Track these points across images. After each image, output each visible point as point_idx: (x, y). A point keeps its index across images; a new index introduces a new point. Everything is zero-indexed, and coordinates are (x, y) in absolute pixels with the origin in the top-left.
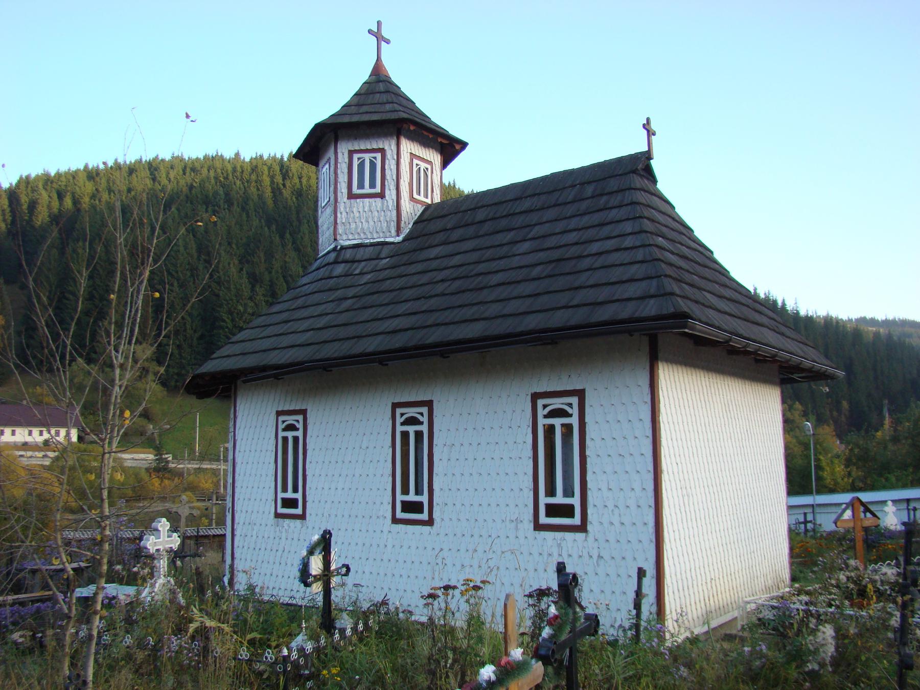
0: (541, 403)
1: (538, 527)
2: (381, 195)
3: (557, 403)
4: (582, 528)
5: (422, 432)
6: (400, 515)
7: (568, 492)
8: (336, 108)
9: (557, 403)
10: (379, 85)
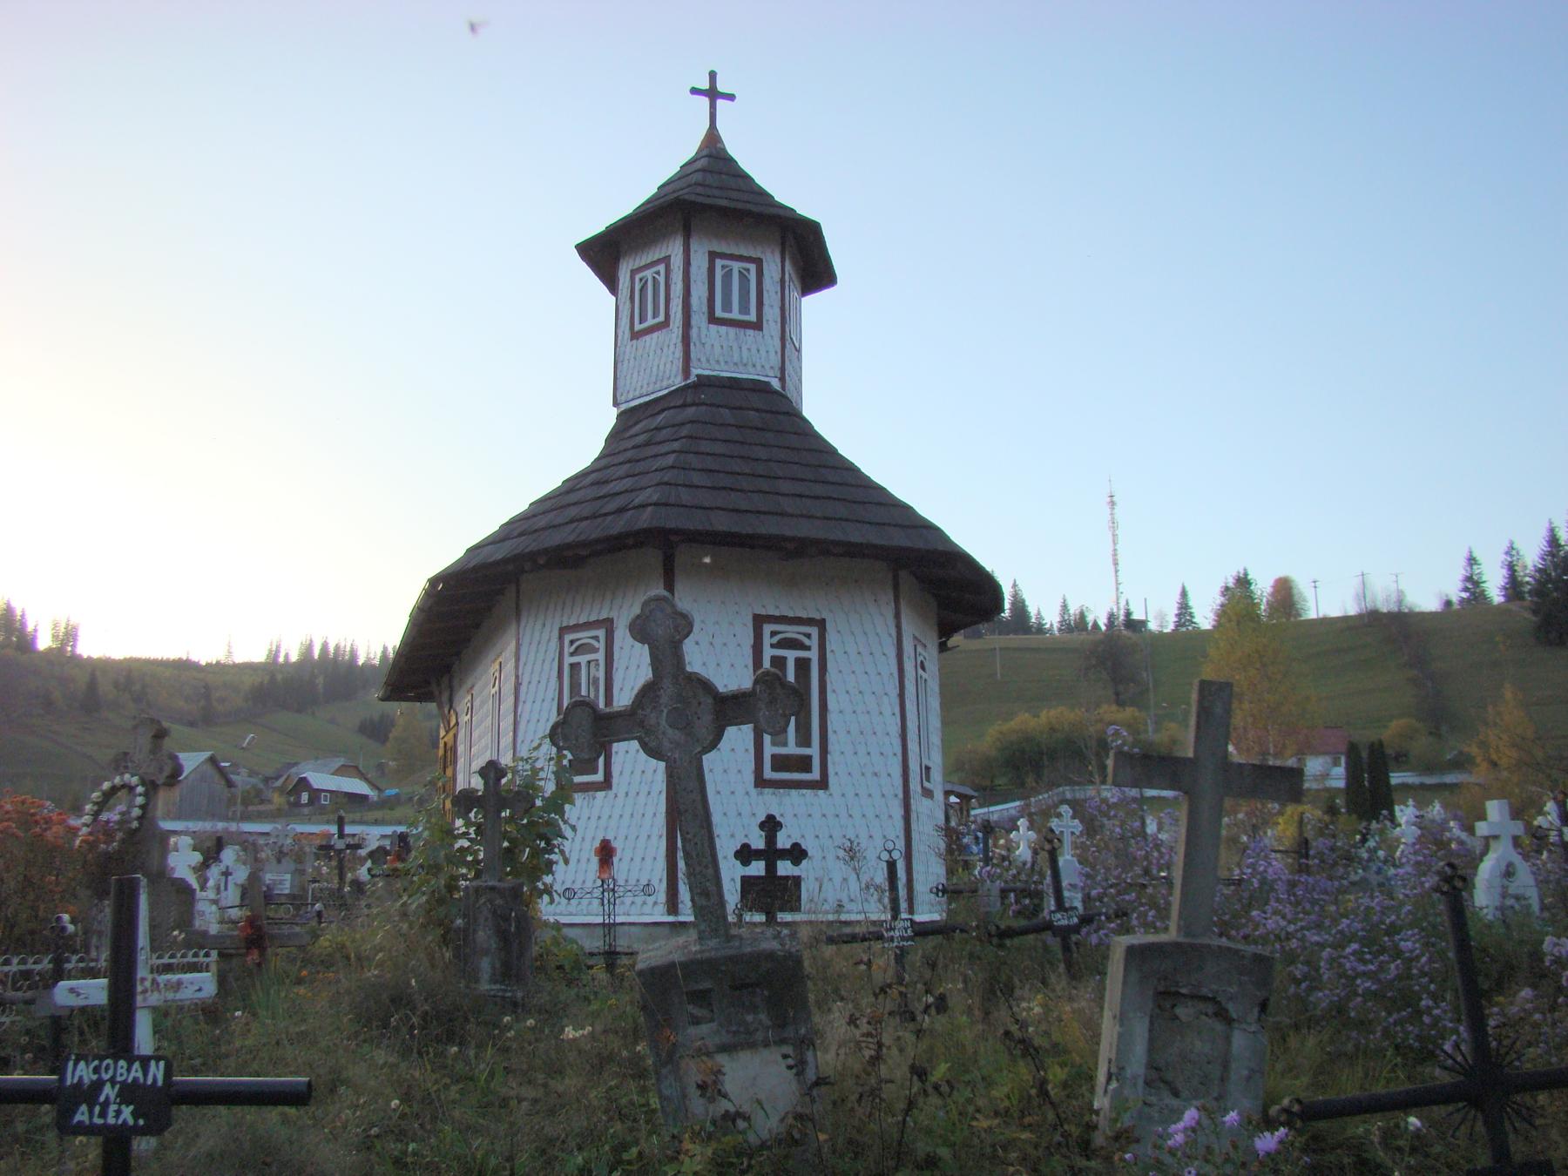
2: (758, 326)
3: (791, 631)
4: (822, 784)
5: (808, 660)
8: (651, 190)
9: (791, 631)
10: (714, 159)
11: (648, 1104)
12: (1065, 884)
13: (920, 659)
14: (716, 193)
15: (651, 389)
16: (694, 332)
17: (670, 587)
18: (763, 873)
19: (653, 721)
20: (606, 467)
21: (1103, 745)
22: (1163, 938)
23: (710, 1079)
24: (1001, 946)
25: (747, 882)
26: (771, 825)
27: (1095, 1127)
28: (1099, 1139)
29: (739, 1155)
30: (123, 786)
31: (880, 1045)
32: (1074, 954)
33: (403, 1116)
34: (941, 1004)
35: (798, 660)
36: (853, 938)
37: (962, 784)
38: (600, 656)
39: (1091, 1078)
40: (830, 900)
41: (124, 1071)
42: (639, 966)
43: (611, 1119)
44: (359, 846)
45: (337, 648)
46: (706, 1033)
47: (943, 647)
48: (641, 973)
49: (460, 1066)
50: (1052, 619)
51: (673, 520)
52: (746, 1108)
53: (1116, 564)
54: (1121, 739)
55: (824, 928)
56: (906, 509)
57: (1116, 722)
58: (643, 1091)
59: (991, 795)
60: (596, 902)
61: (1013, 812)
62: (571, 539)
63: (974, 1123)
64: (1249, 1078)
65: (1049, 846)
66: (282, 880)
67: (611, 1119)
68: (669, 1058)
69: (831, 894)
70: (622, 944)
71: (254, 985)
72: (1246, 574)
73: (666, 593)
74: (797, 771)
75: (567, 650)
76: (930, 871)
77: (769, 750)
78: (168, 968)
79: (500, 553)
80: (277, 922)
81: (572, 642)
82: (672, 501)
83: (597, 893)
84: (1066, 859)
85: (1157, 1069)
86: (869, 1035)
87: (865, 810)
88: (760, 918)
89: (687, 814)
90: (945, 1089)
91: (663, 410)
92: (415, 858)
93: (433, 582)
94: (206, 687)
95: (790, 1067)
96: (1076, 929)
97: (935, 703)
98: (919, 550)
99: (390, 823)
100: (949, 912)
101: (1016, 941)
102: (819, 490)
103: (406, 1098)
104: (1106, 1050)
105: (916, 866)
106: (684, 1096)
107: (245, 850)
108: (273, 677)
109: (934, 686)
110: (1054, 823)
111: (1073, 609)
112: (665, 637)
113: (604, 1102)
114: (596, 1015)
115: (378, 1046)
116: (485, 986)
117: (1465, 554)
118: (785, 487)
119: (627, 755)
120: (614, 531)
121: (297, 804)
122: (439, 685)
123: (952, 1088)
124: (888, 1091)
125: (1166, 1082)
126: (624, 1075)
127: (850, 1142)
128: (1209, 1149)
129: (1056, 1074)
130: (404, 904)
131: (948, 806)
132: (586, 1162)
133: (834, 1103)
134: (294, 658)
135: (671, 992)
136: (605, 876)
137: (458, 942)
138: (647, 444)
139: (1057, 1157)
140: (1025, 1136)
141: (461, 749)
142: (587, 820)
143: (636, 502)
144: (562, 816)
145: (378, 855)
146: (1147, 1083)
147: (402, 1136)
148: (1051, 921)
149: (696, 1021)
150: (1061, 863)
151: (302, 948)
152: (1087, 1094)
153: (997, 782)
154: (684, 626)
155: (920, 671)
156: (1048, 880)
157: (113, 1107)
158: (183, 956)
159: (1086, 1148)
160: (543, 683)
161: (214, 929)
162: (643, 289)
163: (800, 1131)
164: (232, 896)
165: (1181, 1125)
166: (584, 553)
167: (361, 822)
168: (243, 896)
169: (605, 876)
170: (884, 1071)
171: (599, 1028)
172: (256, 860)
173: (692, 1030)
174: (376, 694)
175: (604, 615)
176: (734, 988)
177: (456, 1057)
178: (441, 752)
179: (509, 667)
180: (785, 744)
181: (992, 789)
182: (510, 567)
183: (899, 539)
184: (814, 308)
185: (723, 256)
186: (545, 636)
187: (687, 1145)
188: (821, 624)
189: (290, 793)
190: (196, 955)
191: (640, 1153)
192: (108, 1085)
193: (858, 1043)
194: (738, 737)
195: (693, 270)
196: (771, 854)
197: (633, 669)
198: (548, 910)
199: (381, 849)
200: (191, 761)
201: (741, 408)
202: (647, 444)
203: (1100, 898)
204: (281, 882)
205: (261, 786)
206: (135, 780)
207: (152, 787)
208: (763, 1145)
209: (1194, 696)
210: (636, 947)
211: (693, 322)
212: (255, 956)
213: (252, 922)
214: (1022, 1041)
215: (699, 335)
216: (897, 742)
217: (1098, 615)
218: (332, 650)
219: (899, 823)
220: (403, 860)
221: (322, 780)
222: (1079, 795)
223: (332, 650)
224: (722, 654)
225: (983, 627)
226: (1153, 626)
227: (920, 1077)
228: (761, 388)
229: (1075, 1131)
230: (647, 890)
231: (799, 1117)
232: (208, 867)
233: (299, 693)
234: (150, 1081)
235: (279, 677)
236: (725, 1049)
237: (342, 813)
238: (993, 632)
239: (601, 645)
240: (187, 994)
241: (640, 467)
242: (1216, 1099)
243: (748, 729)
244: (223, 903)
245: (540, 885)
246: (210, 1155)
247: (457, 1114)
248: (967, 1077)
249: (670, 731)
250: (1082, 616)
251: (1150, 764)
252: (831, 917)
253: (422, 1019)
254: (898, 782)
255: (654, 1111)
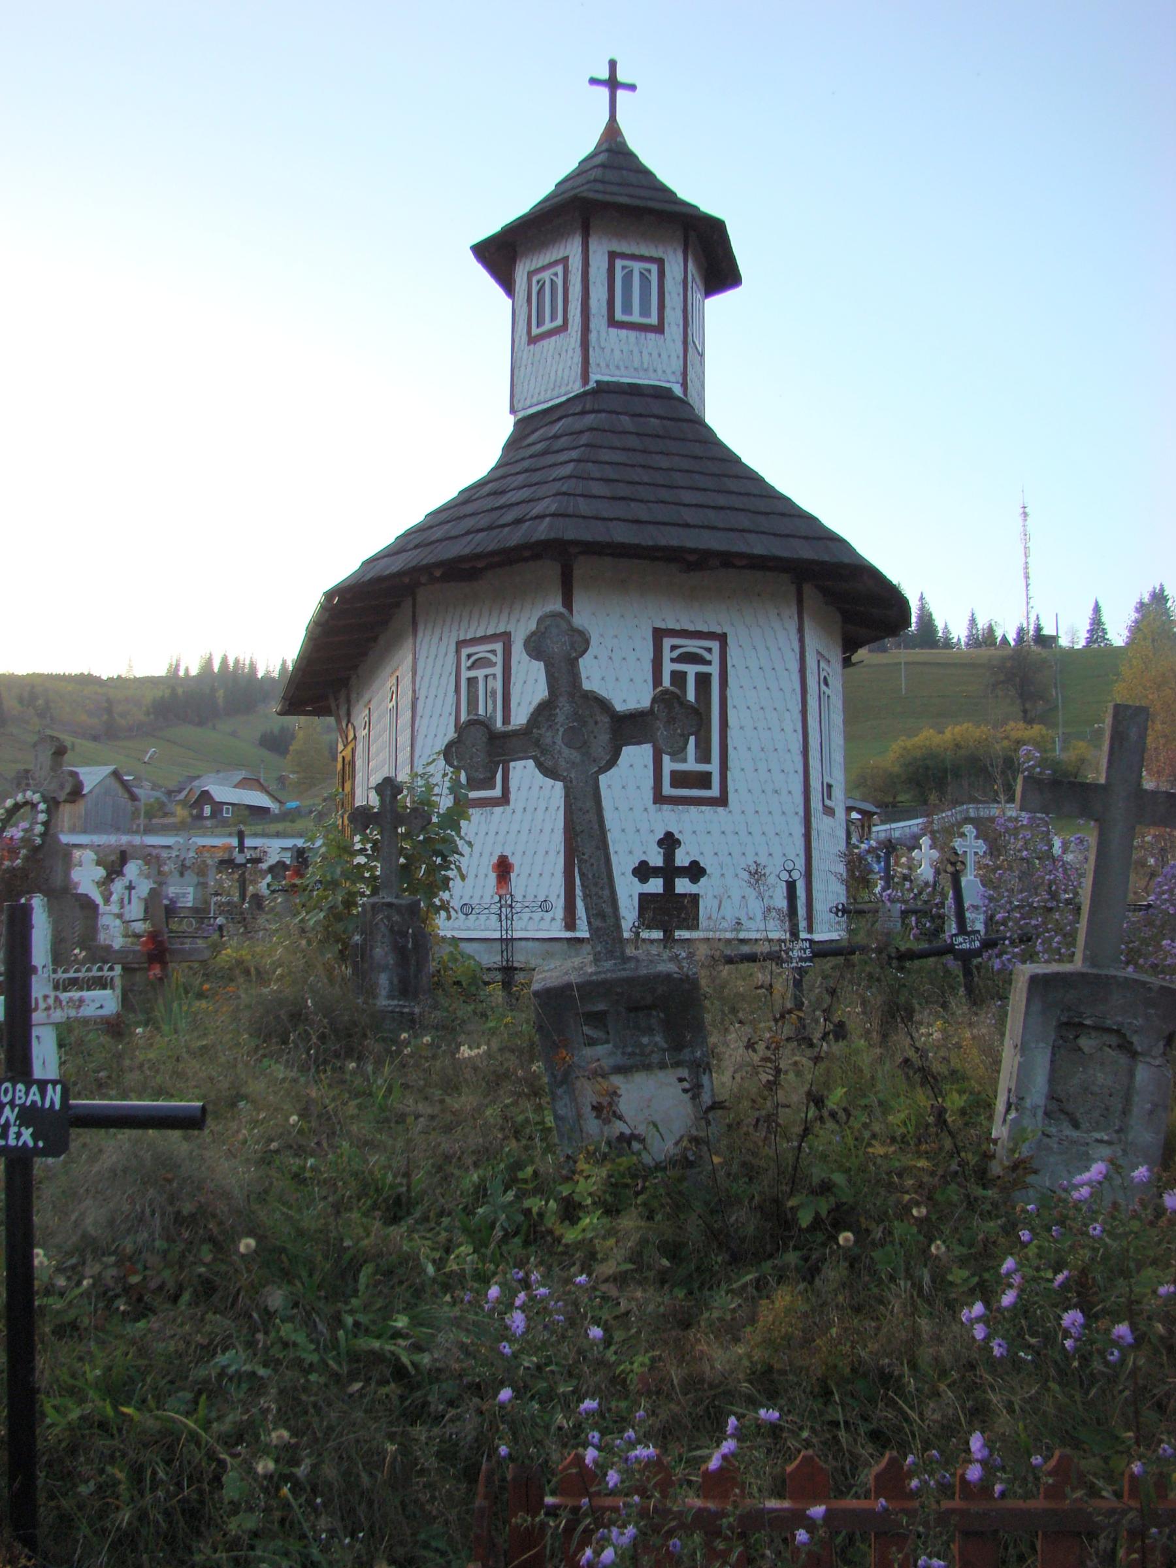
0: (667, 642)
1: (659, 798)
2: (659, 329)
3: (692, 646)
4: (722, 801)
9: (692, 646)
10: (613, 152)
11: (543, 1122)
12: (966, 905)
13: (823, 674)
14: (615, 189)
15: (548, 396)
16: (593, 337)
17: (568, 603)
18: (661, 891)
19: (548, 740)
20: (503, 477)
21: (1010, 765)
22: (1066, 968)
23: (605, 1101)
24: (901, 969)
25: (645, 900)
26: (669, 842)
27: (993, 1156)
28: (996, 1169)
29: (634, 1177)
30: (26, 803)
31: (778, 1071)
32: (973, 977)
33: (301, 1132)
34: (840, 1032)
36: (752, 958)
37: (864, 800)
38: (498, 670)
39: (989, 1106)
40: (728, 918)
41: (22, 1094)
42: (536, 986)
43: (506, 1138)
44: (259, 860)
45: (237, 661)
46: (601, 1054)
47: (847, 662)
48: (536, 994)
49: (358, 1081)
50: (959, 632)
51: (571, 531)
52: (641, 1130)
53: (1027, 577)
54: (1028, 756)
55: (721, 946)
56: (811, 520)
57: (1028, 741)
58: (539, 1109)
59: (893, 812)
60: (494, 918)
61: (915, 829)
62: (467, 551)
63: (870, 1150)
64: (1151, 1112)
65: (952, 867)
66: (184, 893)
67: (506, 1138)
68: (564, 1079)
69: (730, 912)
70: (519, 960)
71: (156, 999)
72: (1162, 590)
73: (562, 610)
74: (698, 788)
75: (465, 663)
76: (830, 890)
77: (668, 765)
78: (73, 983)
79: (397, 564)
80: (183, 935)
81: (469, 656)
82: (570, 511)
83: (495, 909)
84: (970, 880)
85: (1059, 1100)
86: (766, 1059)
87: (764, 831)
88: (657, 935)
89: (585, 839)
90: (842, 1116)
91: (559, 419)
92: (313, 873)
93: (329, 595)
94: (108, 701)
95: (685, 1091)
96: (977, 953)
97: (837, 719)
98: (823, 563)
99: (292, 836)
100: (850, 931)
101: (917, 963)
102: (721, 500)
103: (304, 1115)
104: (1005, 1081)
105: (816, 885)
106: (579, 1116)
107: (147, 863)
108: (173, 689)
109: (837, 702)
110: (957, 843)
111: (982, 624)
112: (561, 653)
113: (500, 1121)
114: (493, 1032)
115: (277, 1062)
116: (383, 1002)
118: (688, 497)
119: (524, 773)
120: (512, 543)
121: (200, 817)
122: (336, 699)
123: (849, 1115)
124: (784, 1116)
125: (1067, 1114)
126: (520, 1095)
127: (744, 1164)
128: (1115, 1205)
129: (955, 1101)
130: (302, 921)
131: (849, 822)
132: (483, 1180)
133: (729, 1126)
134: (194, 672)
135: (564, 1013)
136: (502, 892)
137: (356, 957)
138: (545, 453)
139: (953, 1186)
140: (922, 1163)
141: (358, 763)
142: (482, 836)
143: (534, 512)
144: (458, 834)
145: (278, 869)
146: (1047, 1114)
147: (300, 1151)
148: (952, 945)
149: (592, 1042)
150: (963, 884)
151: (203, 962)
152: (985, 1123)
153: (899, 799)
154: (581, 642)
155: (823, 687)
156: (950, 901)
157: (13, 1130)
158: (89, 970)
159: (982, 1176)
160: (441, 696)
161: (118, 943)
162: (540, 292)
163: (694, 1154)
164: (135, 910)
165: (1086, 1176)
166: (480, 565)
167: (264, 835)
168: (146, 911)
169: (502, 892)
170: (781, 1096)
171: (495, 1045)
172: (160, 873)
173: (588, 1052)
174: (275, 707)
175: (501, 629)
176: (630, 1010)
177: (353, 1073)
178: (339, 766)
179: (406, 681)
180: (685, 760)
181: (894, 806)
182: (406, 580)
183: (805, 552)
184: (718, 310)
185: (624, 256)
186: (443, 650)
187: (582, 1165)
188: (722, 638)
189: (193, 806)
190: (100, 969)
191: (536, 1174)
192: (8, 1108)
193: (754, 1067)
194: (636, 759)
195: (592, 271)
196: (669, 872)
197: (530, 686)
198: (445, 927)
199: (281, 865)
200: (92, 777)
201: (641, 415)
202: (545, 453)
203: (1004, 923)
204: (184, 895)
205: (164, 799)
206: (36, 797)
207: (53, 804)
208: (659, 1167)
209: (1109, 720)
210: (533, 963)
211: (592, 326)
212: (157, 971)
213: (154, 936)
214: (921, 1069)
215: (598, 339)
216: (799, 760)
217: (1008, 630)
218: (231, 663)
219: (800, 842)
220: (302, 876)
221: (223, 792)
222: (984, 813)
223: (231, 663)
224: (620, 671)
225: (889, 642)
226: (1064, 642)
227: (816, 1105)
228: (661, 394)
229: (972, 1159)
230: (545, 906)
231: (695, 1140)
232: (112, 881)
233: (197, 705)
234: (47, 1105)
235: (180, 691)
236: (620, 1070)
237: (243, 827)
238: (898, 646)
239: (499, 659)
240: (88, 1011)
241: (537, 477)
242: (1117, 1132)
243: (647, 750)
244: (127, 917)
245: (437, 901)
246: (113, 1171)
247: (354, 1128)
248: (863, 1102)
249: (566, 751)
250: (991, 630)
251: (1063, 792)
252: (729, 935)
253: (326, 1036)
254: (800, 799)
255: (550, 1129)
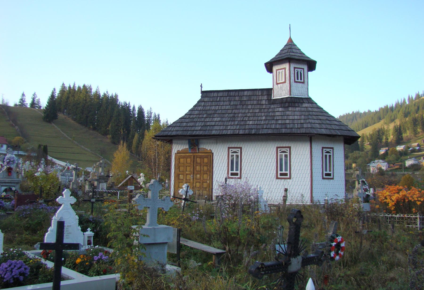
0: (230, 150)
1: (323, 178)
2: (303, 83)
3: (328, 150)
4: (240, 178)
6: (288, 177)
7: (286, 170)
8: (278, 51)
9: (328, 150)
10: (290, 45)
35: (236, 155)
117: (22, 93)
188: (332, 148)
